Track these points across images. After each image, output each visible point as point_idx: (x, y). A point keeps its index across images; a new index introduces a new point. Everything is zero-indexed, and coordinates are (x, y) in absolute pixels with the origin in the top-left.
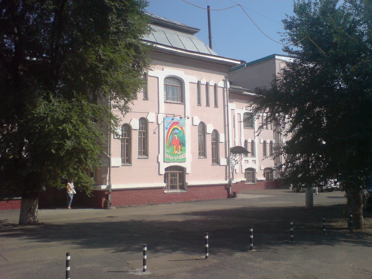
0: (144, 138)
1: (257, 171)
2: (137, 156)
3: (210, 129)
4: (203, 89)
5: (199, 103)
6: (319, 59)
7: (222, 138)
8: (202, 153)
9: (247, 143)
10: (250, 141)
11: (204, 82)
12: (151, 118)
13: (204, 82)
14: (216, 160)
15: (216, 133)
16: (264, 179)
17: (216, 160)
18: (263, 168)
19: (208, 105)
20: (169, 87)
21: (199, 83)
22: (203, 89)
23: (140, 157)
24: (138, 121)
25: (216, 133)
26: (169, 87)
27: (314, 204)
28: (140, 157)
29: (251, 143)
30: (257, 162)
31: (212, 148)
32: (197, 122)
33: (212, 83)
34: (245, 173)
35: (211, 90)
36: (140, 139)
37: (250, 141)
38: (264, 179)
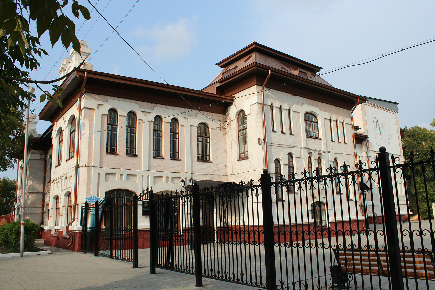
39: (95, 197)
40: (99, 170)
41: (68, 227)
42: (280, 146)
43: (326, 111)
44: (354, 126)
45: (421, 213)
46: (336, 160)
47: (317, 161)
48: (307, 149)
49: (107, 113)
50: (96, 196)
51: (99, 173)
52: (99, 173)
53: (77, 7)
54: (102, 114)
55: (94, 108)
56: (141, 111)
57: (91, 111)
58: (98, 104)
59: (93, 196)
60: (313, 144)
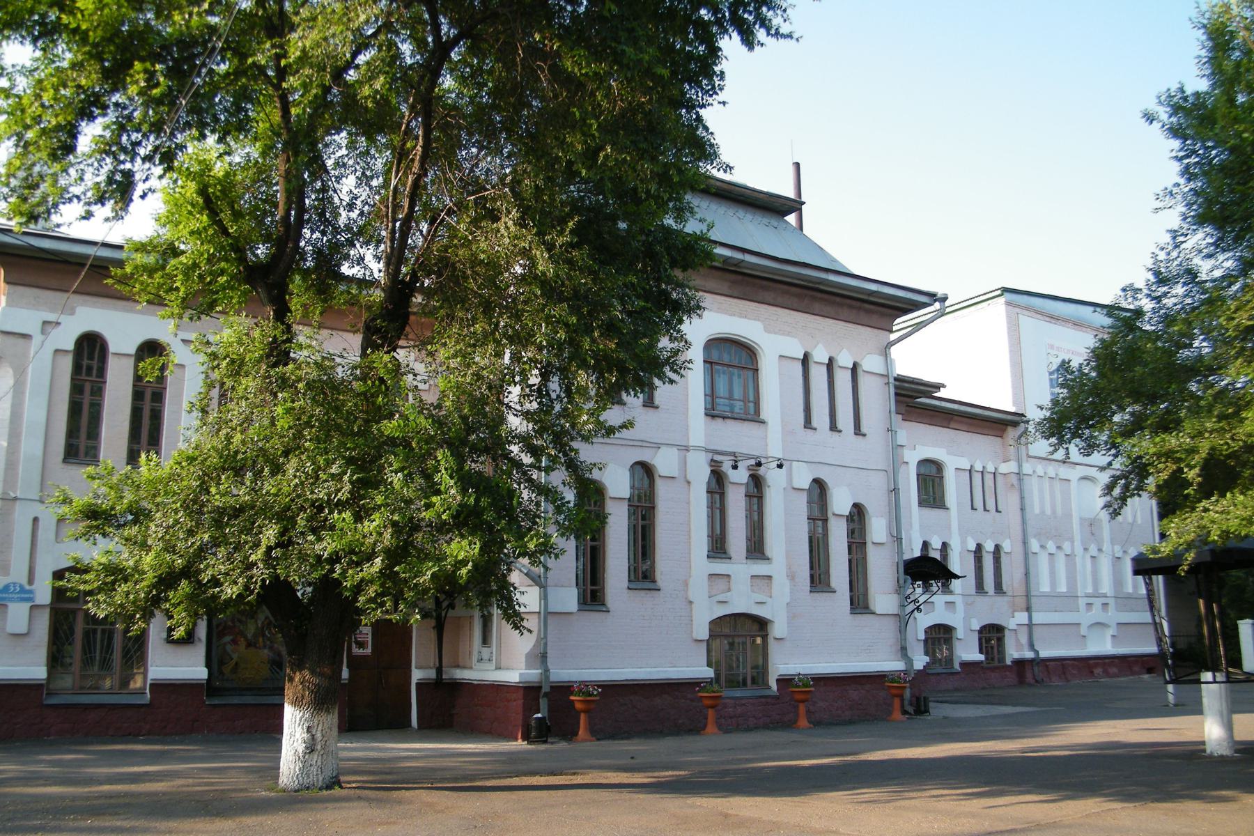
0: (644, 527)
1: (960, 633)
2: (625, 583)
3: (841, 503)
4: (819, 376)
5: (808, 423)
6: (277, 148)
7: (877, 529)
8: (819, 580)
9: (726, 484)
10: (989, 547)
11: (820, 355)
12: (664, 462)
13: (820, 355)
14: (859, 603)
15: (858, 514)
16: (982, 657)
17: (859, 603)
18: (976, 626)
19: (834, 427)
20: (718, 371)
21: (806, 360)
22: (819, 376)
23: (632, 586)
24: (628, 473)
25: (858, 514)
26: (718, 371)
27: (892, 665)
28: (632, 586)
29: (850, 518)
30: (960, 606)
31: (850, 561)
32: (803, 479)
33: (845, 360)
34: (926, 641)
35: (843, 380)
36: (633, 529)
37: (989, 547)
38: (982, 657)
39: (21, 586)
40: (38, 510)
41: (126, 805)
42: (640, 444)
43: (789, 334)
44: (899, 379)
45: (446, 469)
46: (819, 486)
47: (801, 503)
48: (707, 451)
49: (70, 346)
50: (24, 581)
51: (36, 520)
52: (36, 520)
53: (703, 12)
54: (57, 351)
55: (30, 333)
56: (183, 340)
57: (21, 341)
58: (45, 323)
59: (14, 583)
60: (735, 437)
